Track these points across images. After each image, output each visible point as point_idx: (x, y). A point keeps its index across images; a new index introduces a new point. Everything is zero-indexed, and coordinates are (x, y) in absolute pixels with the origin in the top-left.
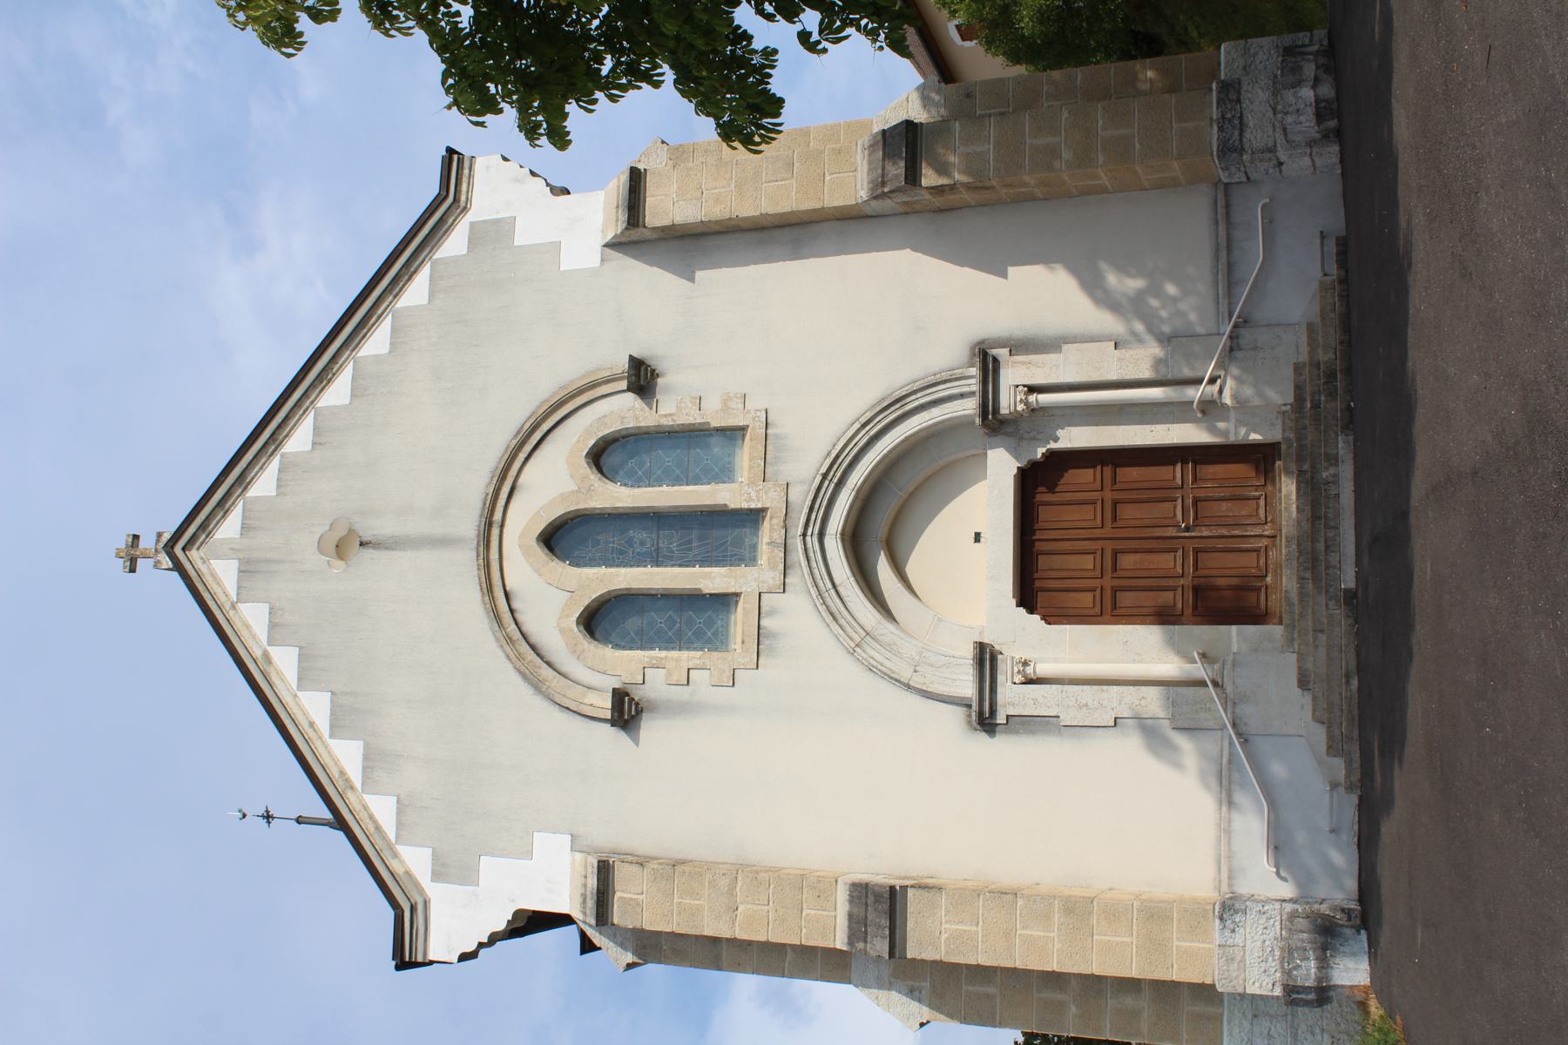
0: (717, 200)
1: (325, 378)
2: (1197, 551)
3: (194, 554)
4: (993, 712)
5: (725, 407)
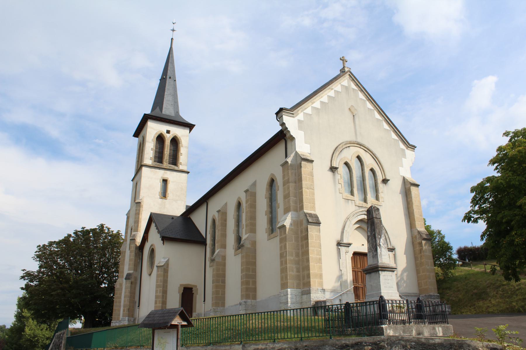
1: (379, 113)
3: (348, 76)
5: (382, 198)
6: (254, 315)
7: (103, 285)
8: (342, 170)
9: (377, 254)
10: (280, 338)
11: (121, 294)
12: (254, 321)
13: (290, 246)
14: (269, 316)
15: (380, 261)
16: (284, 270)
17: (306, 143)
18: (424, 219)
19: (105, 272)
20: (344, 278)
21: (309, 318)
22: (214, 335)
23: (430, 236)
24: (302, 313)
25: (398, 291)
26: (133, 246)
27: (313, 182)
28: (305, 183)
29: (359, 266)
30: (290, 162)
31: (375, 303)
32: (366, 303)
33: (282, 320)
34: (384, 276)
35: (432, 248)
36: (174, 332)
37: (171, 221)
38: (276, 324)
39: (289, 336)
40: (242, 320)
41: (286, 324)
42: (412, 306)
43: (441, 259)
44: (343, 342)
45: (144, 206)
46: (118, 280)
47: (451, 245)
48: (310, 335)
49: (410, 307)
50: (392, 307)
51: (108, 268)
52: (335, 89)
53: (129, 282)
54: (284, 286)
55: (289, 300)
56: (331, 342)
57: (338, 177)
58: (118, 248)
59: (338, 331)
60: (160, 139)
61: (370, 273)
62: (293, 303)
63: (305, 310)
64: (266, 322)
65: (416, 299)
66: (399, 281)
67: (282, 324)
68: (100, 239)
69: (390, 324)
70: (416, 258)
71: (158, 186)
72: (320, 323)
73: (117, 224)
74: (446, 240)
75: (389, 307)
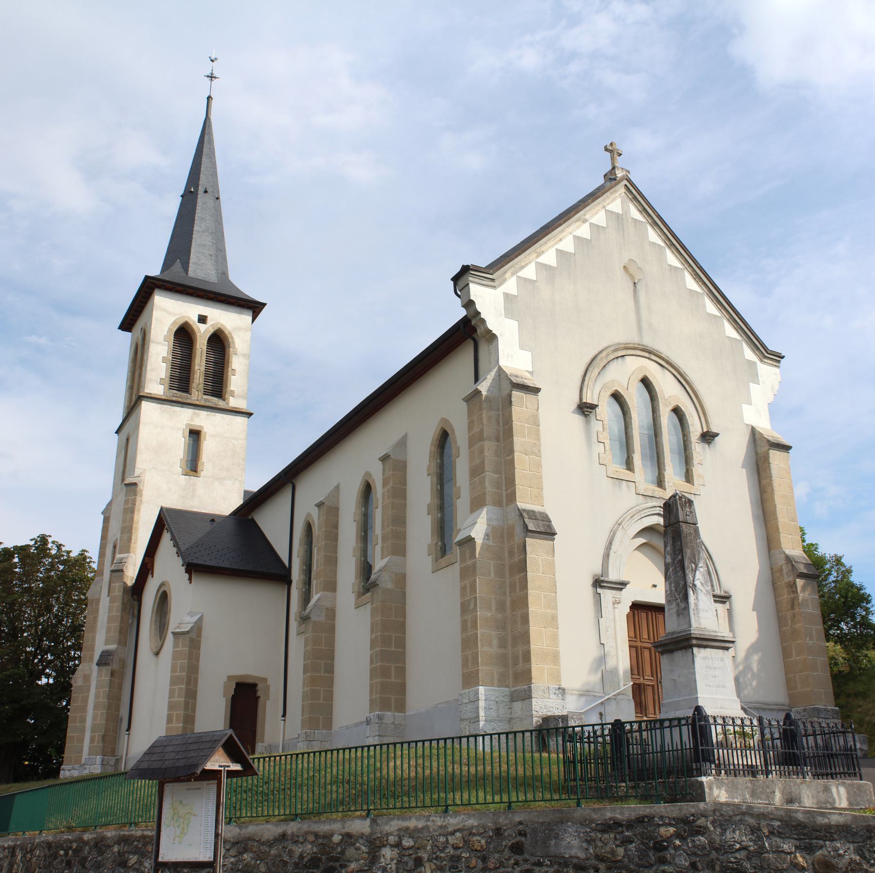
0: (780, 485)
1: (696, 277)
2: (653, 686)
4: (602, 587)
5: (700, 476)
6: (398, 746)
7: (44, 681)
8: (607, 410)
9: (687, 608)
10: (459, 802)
11: (85, 700)
12: (399, 762)
13: (483, 586)
14: (435, 751)
15: (694, 624)
16: (469, 643)
17: (522, 347)
18: (802, 530)
19: (49, 650)
20: (611, 663)
21: (528, 755)
22: (305, 796)
23: (816, 568)
24: (511, 743)
25: (739, 696)
26: (117, 585)
27: (538, 437)
28: (519, 441)
29: (645, 636)
30: (484, 393)
31: (683, 722)
32: (662, 721)
33: (465, 761)
34: (704, 658)
35: (821, 597)
36: (212, 786)
37: (208, 527)
38: (450, 769)
39: (481, 800)
40: (372, 761)
41: (473, 770)
42: (772, 734)
43: (843, 625)
44: (609, 815)
45: (145, 493)
46: (79, 668)
47: (868, 591)
48: (530, 796)
49: (768, 736)
50: (725, 733)
51: (56, 639)
52: (592, 221)
53: (106, 670)
54: (470, 679)
55: (482, 713)
56: (579, 813)
57: (596, 426)
58: (82, 591)
59: (596, 788)
60: (184, 335)
61: (671, 651)
62: (490, 721)
63: (519, 736)
64: (427, 764)
65: (781, 716)
66: (740, 673)
67: (465, 768)
68: (38, 571)
69: (719, 773)
70: (781, 621)
71: (179, 445)
72: (554, 767)
73: (78, 535)
74: (855, 579)
75: (716, 733)
